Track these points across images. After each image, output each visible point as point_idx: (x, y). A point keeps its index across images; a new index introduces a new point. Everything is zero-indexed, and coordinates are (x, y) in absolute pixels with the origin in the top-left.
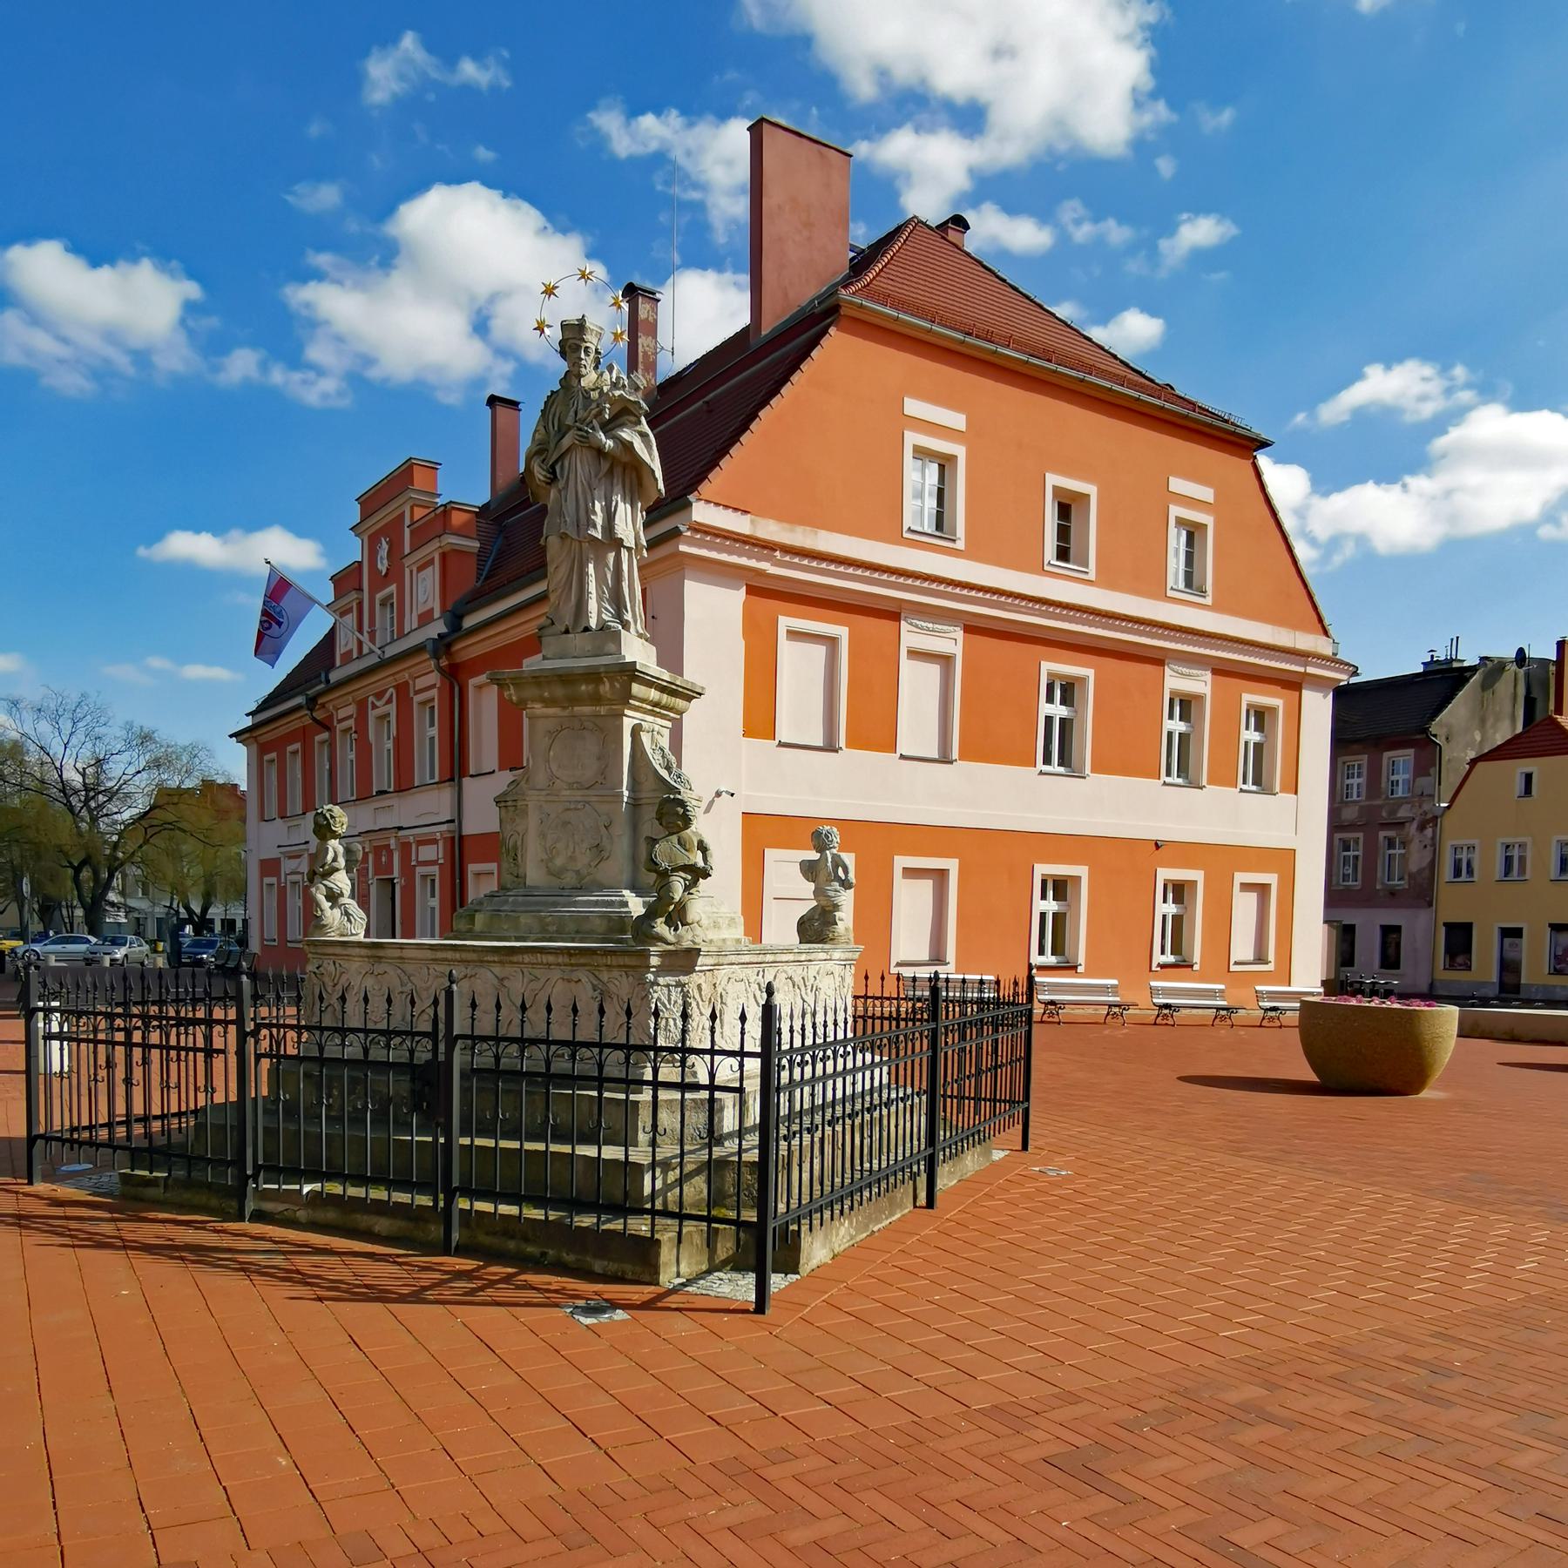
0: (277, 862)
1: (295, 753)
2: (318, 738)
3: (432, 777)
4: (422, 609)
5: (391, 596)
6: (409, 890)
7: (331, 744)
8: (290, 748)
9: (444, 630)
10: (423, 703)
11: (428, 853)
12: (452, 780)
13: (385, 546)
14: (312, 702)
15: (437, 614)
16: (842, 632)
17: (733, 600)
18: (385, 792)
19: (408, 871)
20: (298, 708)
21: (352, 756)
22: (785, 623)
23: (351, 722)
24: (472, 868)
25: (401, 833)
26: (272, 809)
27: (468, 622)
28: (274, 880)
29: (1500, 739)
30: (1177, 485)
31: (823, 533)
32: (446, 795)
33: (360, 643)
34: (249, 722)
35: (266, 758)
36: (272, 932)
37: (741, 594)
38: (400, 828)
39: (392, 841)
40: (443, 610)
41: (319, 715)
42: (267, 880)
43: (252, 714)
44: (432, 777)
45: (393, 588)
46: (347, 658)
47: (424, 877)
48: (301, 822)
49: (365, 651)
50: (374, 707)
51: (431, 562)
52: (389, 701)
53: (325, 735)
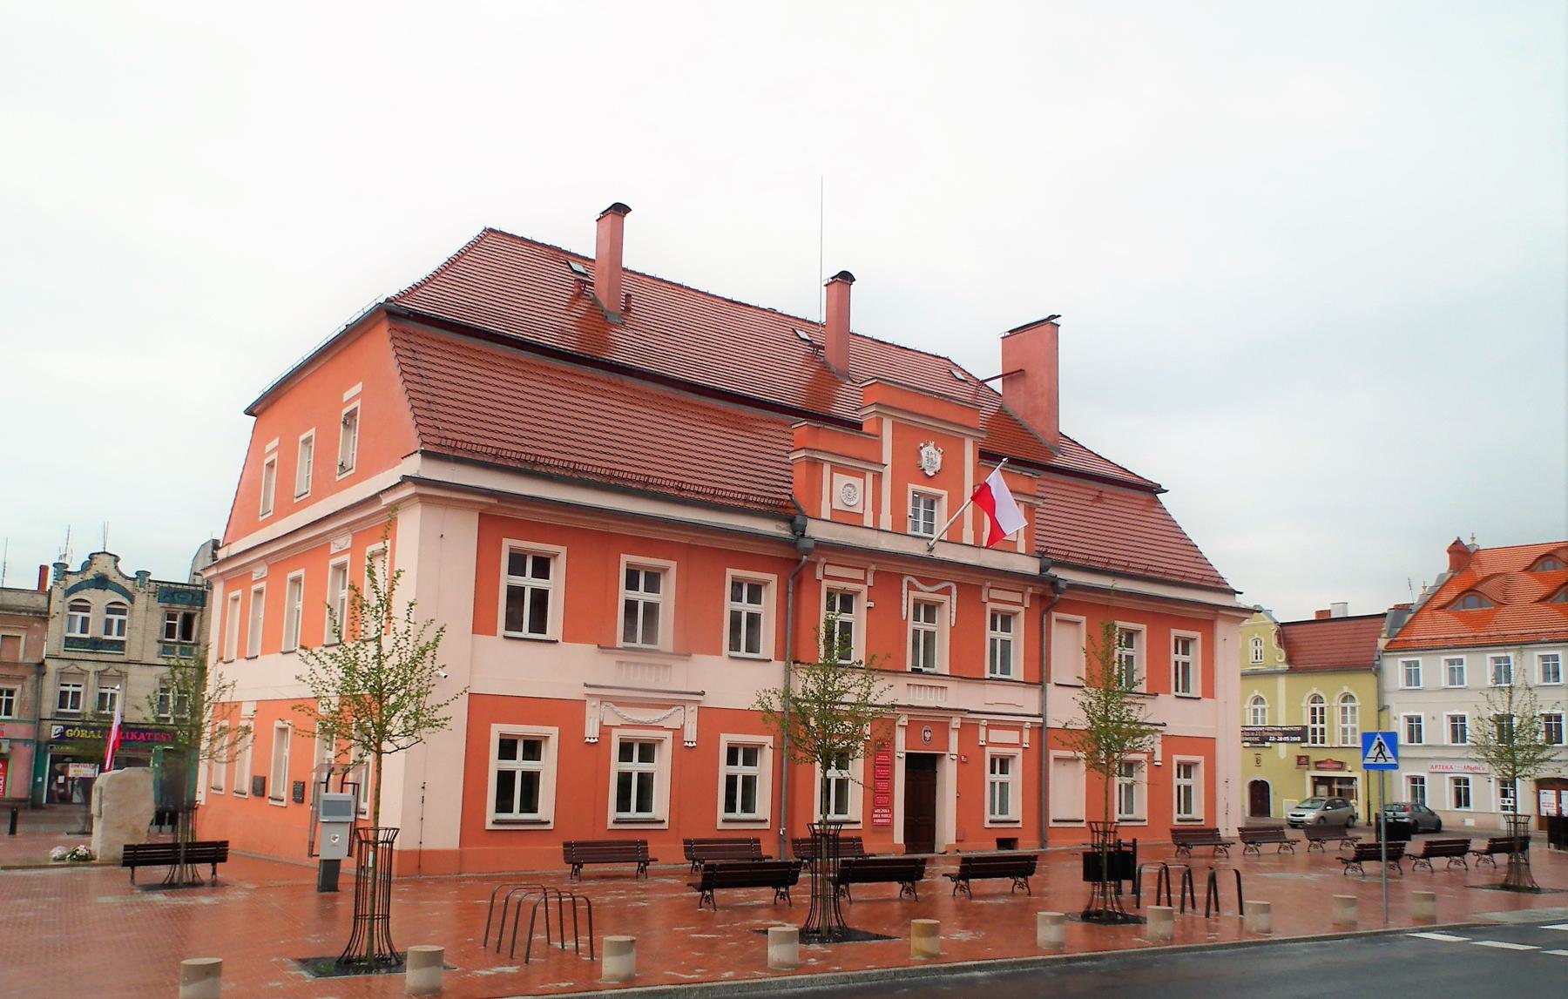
16: (1083, 619)
24: (1053, 753)
35: (232, 595)
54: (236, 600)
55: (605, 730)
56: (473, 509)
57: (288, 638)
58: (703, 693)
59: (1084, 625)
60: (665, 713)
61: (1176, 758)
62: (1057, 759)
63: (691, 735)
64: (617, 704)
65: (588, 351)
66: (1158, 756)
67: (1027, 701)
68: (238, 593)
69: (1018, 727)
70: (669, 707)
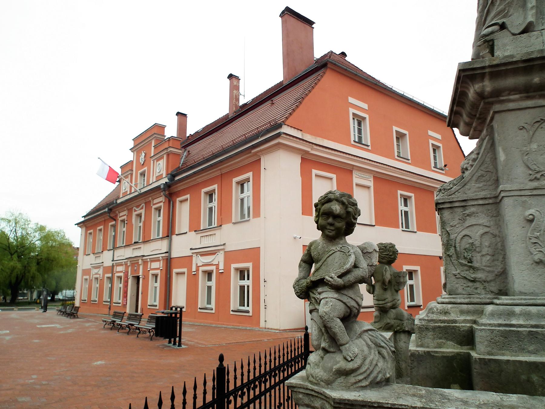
0: (90, 270)
1: (100, 230)
2: (110, 224)
3: (158, 235)
4: (158, 174)
5: (145, 171)
6: (146, 278)
7: (114, 226)
8: (99, 228)
9: (167, 181)
10: (156, 209)
11: (155, 265)
12: (168, 236)
13: (143, 154)
14: (110, 210)
15: (164, 176)
16: (334, 176)
17: (295, 162)
18: (137, 242)
19: (146, 272)
20: (105, 212)
21: (91, 241)
22: (314, 172)
23: (125, 217)
24: (175, 271)
25: (144, 258)
26: (89, 251)
27: (177, 178)
28: (87, 277)
29: (23, 282)
30: (430, 133)
31: (326, 141)
32: (165, 242)
33: (131, 187)
34: (83, 219)
35: (89, 232)
36: (85, 297)
37: (299, 161)
38: (143, 256)
39: (140, 261)
40: (167, 174)
41: (112, 215)
42: (85, 277)
43: (84, 217)
44: (123, 244)
45: (146, 168)
46: (125, 194)
47: (118, 277)
48: (101, 255)
49: (133, 191)
50: (135, 211)
51: (163, 158)
52: (142, 208)
53: (114, 223)
54: (90, 234)
55: (198, 267)
56: (299, 154)
57: (110, 245)
58: (224, 244)
59: (335, 180)
60: (212, 257)
61: (234, 266)
62: (178, 274)
63: (221, 267)
64: (202, 255)
65: (302, 69)
66: (221, 267)
67: (161, 247)
68: (92, 231)
69: (157, 260)
70: (214, 254)
